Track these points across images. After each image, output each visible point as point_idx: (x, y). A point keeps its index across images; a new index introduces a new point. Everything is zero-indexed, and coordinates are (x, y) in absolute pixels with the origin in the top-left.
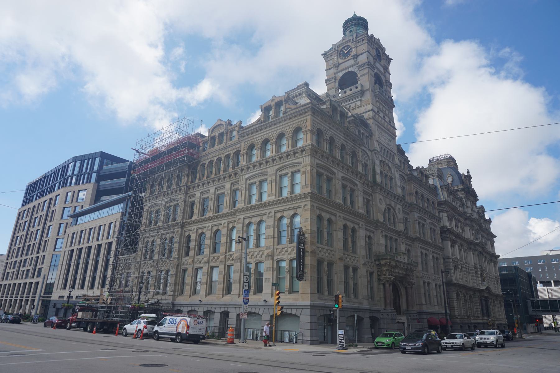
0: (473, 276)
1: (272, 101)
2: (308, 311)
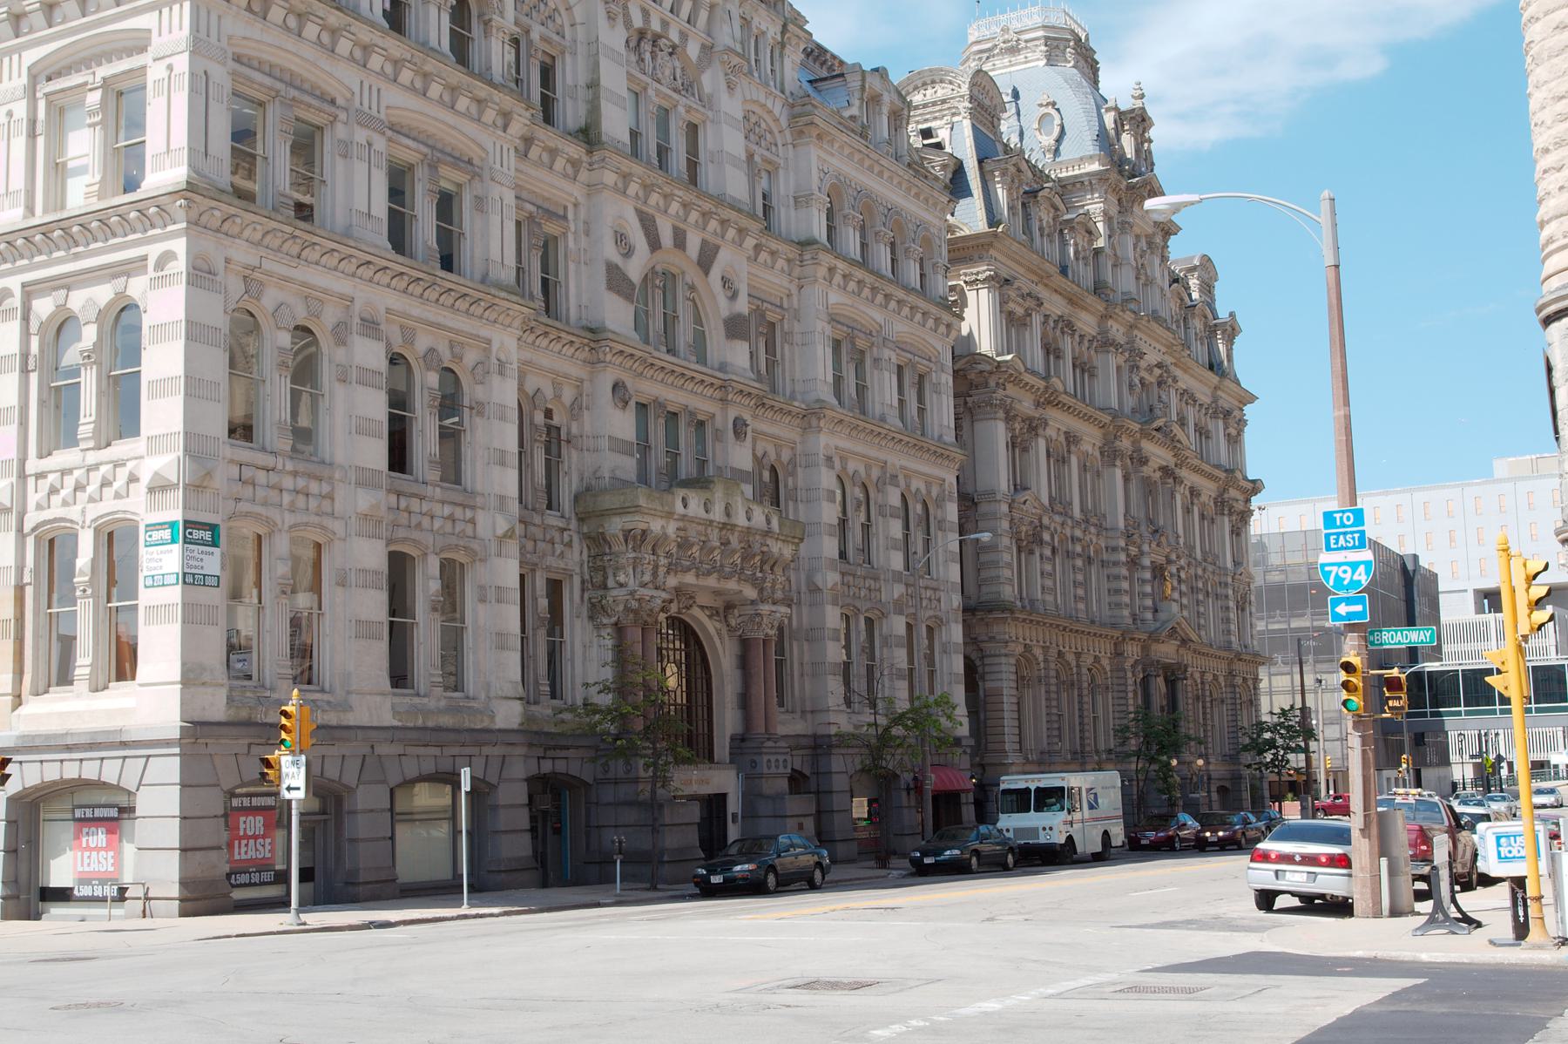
0: (1117, 577)
2: (168, 768)
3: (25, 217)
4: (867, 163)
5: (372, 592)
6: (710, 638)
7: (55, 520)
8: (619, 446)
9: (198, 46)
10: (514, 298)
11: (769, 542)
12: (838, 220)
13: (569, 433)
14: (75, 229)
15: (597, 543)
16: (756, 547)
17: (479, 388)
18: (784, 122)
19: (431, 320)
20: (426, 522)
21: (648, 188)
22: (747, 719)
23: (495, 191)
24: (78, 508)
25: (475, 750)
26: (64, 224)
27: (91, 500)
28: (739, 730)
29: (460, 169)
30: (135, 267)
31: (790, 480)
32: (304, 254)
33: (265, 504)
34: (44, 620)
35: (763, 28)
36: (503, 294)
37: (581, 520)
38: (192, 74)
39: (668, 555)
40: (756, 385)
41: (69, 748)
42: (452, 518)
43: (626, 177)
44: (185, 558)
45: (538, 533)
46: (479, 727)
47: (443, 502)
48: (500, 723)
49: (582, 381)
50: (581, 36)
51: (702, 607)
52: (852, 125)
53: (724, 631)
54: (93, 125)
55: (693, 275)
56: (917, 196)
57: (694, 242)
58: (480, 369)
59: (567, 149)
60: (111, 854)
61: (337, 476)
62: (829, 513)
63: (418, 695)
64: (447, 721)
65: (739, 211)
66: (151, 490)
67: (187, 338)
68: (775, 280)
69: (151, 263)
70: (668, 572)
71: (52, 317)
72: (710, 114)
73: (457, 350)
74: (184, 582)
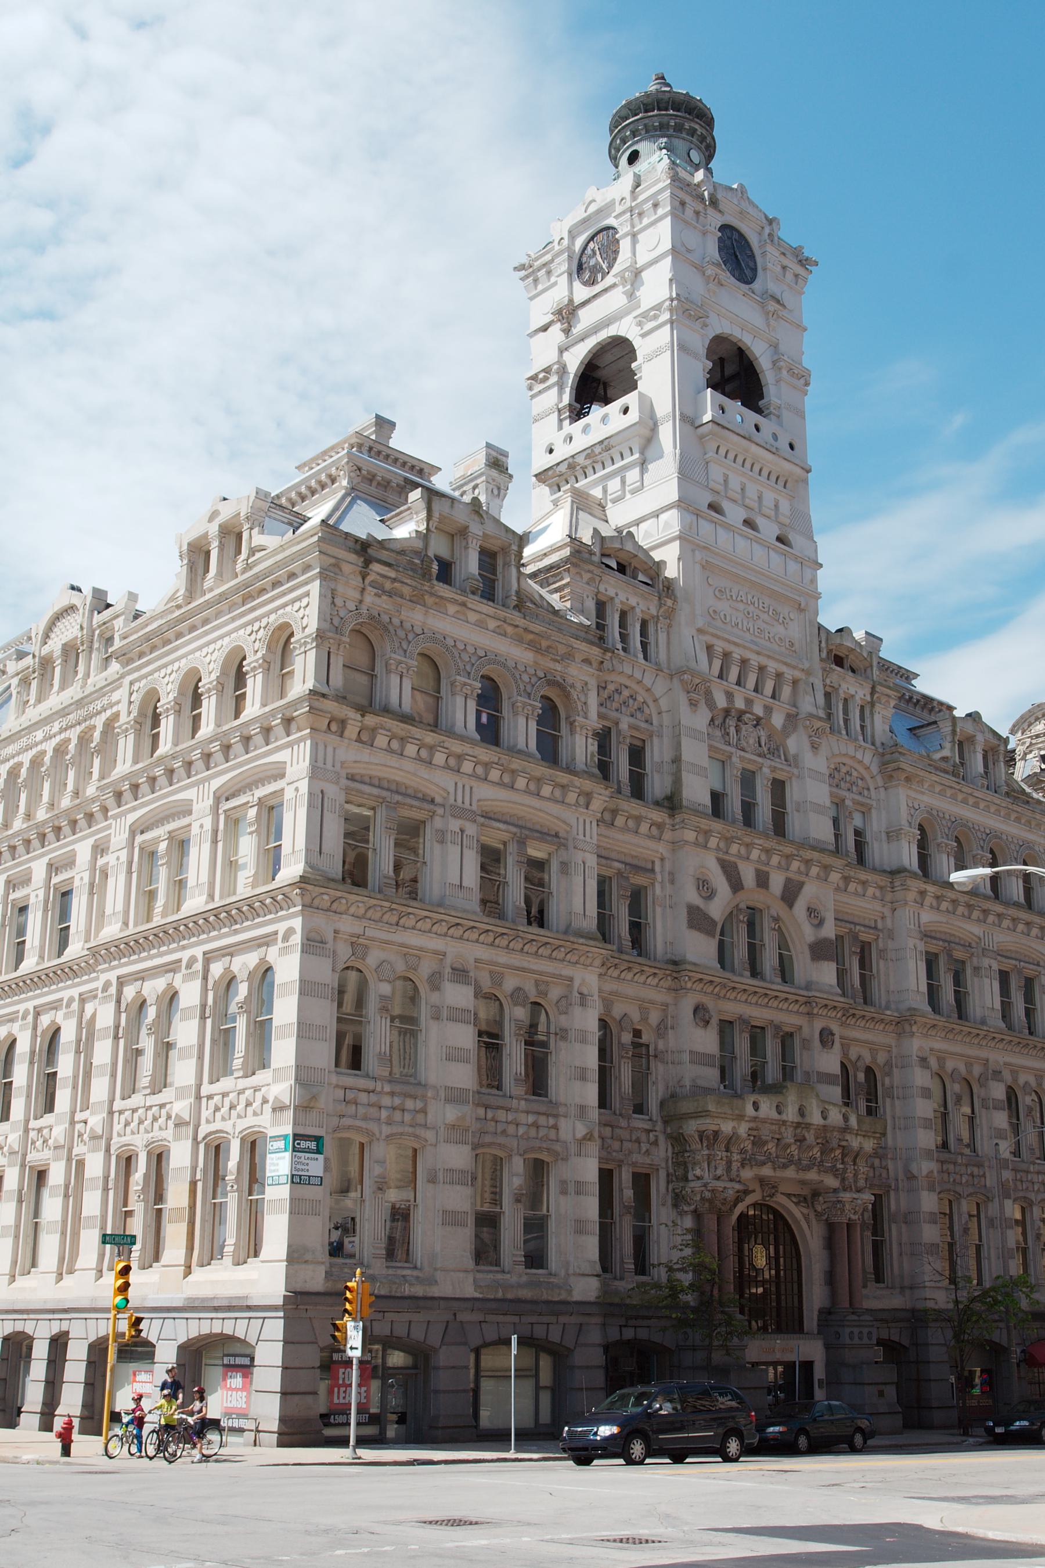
1: (211, 520)
2: (275, 1328)
3: (207, 903)
4: (960, 797)
5: (458, 1187)
6: (797, 1222)
7: (217, 1132)
8: (699, 1059)
9: (316, 772)
10: (592, 943)
11: (848, 1137)
12: (932, 850)
13: (656, 1049)
14: (234, 912)
15: (678, 1141)
16: (834, 1143)
17: (563, 1017)
18: (874, 769)
19: (519, 964)
20: (511, 1129)
21: (729, 841)
22: (833, 1294)
23: (579, 857)
24: (231, 1122)
25: (553, 1319)
26: (227, 908)
27: (239, 1117)
28: (827, 1304)
29: (546, 842)
30: (266, 941)
31: (887, 1080)
32: (402, 921)
33: (365, 1118)
34: (209, 1208)
35: (852, 691)
36: (581, 941)
37: (666, 1122)
38: (310, 794)
39: (742, 1151)
40: (842, 999)
41: (216, 1309)
42: (536, 1125)
43: (707, 833)
44: (293, 1163)
45: (625, 1134)
46: (556, 1299)
47: (528, 1112)
48: (577, 1296)
49: (667, 1005)
50: (666, 719)
51: (788, 1196)
52: (943, 765)
53: (812, 1216)
54: (251, 833)
55: (778, 908)
56: (1018, 820)
57: (777, 882)
58: (563, 1002)
59: (650, 815)
60: (245, 1394)
61: (429, 1094)
62: (925, 1108)
63: (503, 1272)
64: (525, 1294)
65: (822, 851)
66: (274, 1110)
67: (300, 994)
68: (865, 905)
69: (184, 964)
70: (743, 1165)
71: (222, 977)
72: (795, 771)
73: (542, 988)
74: (292, 1182)
